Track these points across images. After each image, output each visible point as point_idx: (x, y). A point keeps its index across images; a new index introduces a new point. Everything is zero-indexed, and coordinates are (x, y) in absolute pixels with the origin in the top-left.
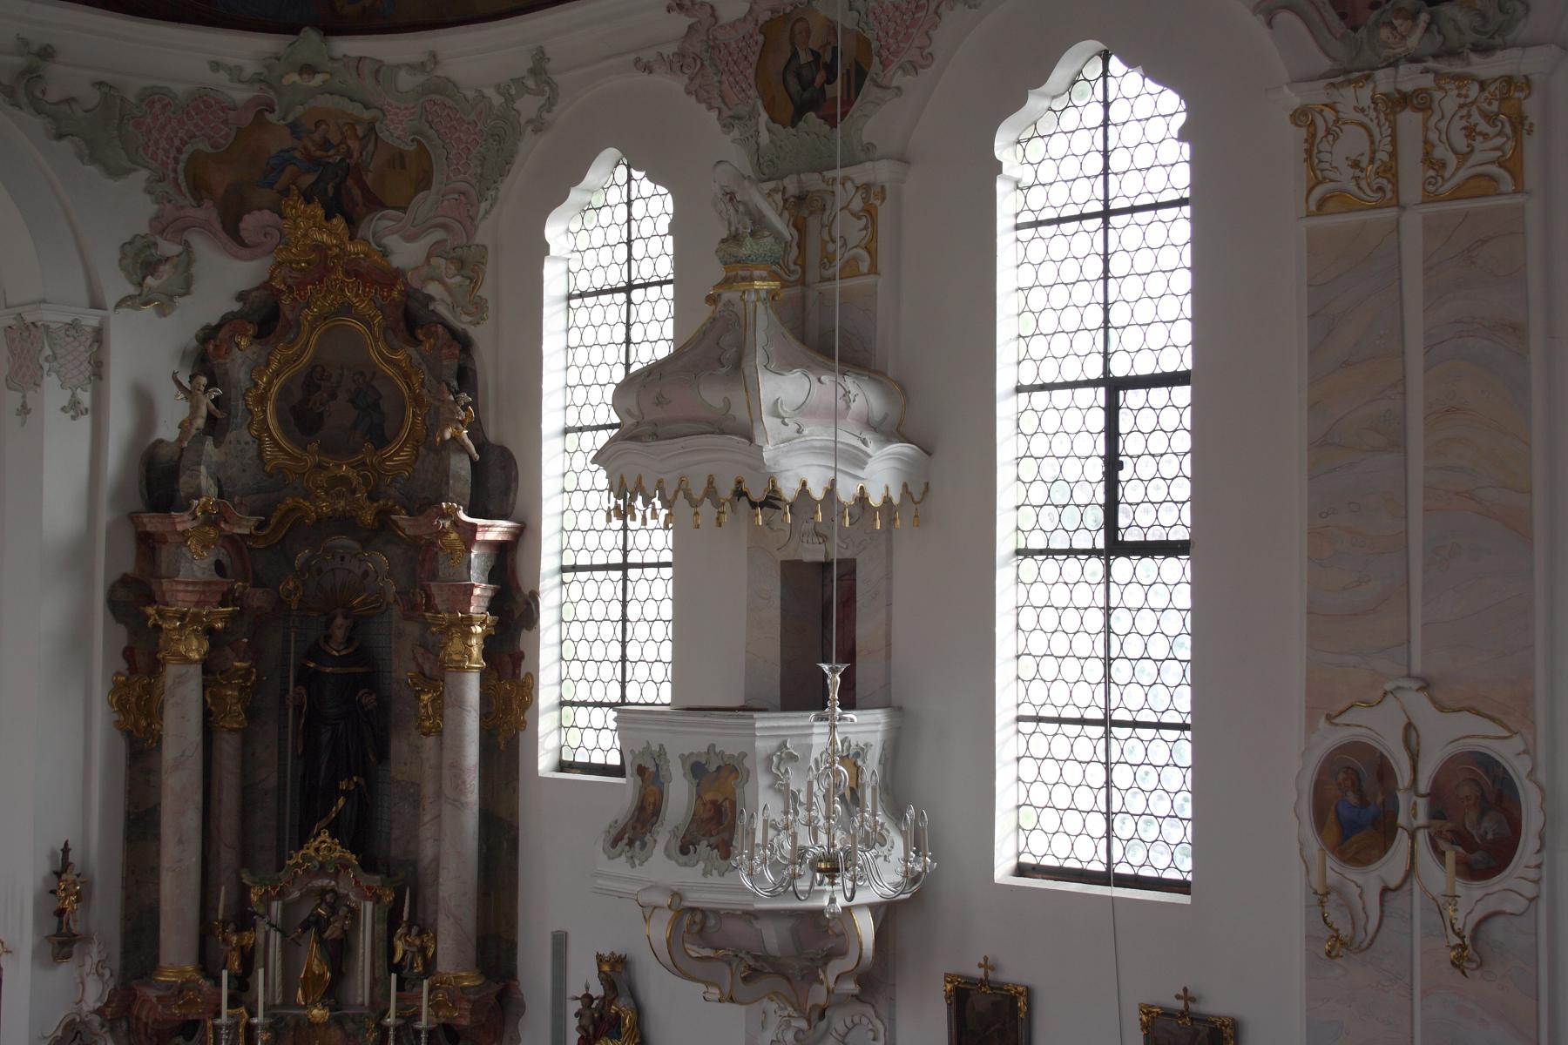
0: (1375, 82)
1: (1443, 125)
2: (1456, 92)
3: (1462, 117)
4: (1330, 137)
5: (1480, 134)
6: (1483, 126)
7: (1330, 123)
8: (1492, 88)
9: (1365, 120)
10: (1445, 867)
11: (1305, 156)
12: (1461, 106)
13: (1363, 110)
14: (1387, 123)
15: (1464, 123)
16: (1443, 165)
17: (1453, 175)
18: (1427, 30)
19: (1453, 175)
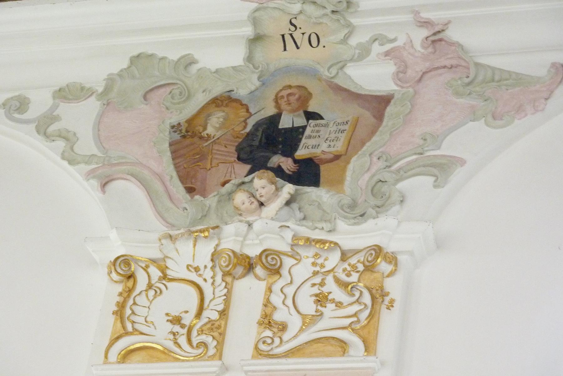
0: (219, 239)
1: (290, 291)
2: (312, 260)
3: (314, 285)
4: (151, 293)
5: (333, 301)
6: (338, 294)
7: (154, 279)
8: (353, 261)
9: (199, 281)
10: (321, 118)
11: (116, 309)
12: (315, 273)
13: (197, 269)
14: (224, 284)
15: (316, 290)
16: (283, 327)
17: (295, 337)
18: (288, 203)
19: (295, 337)
